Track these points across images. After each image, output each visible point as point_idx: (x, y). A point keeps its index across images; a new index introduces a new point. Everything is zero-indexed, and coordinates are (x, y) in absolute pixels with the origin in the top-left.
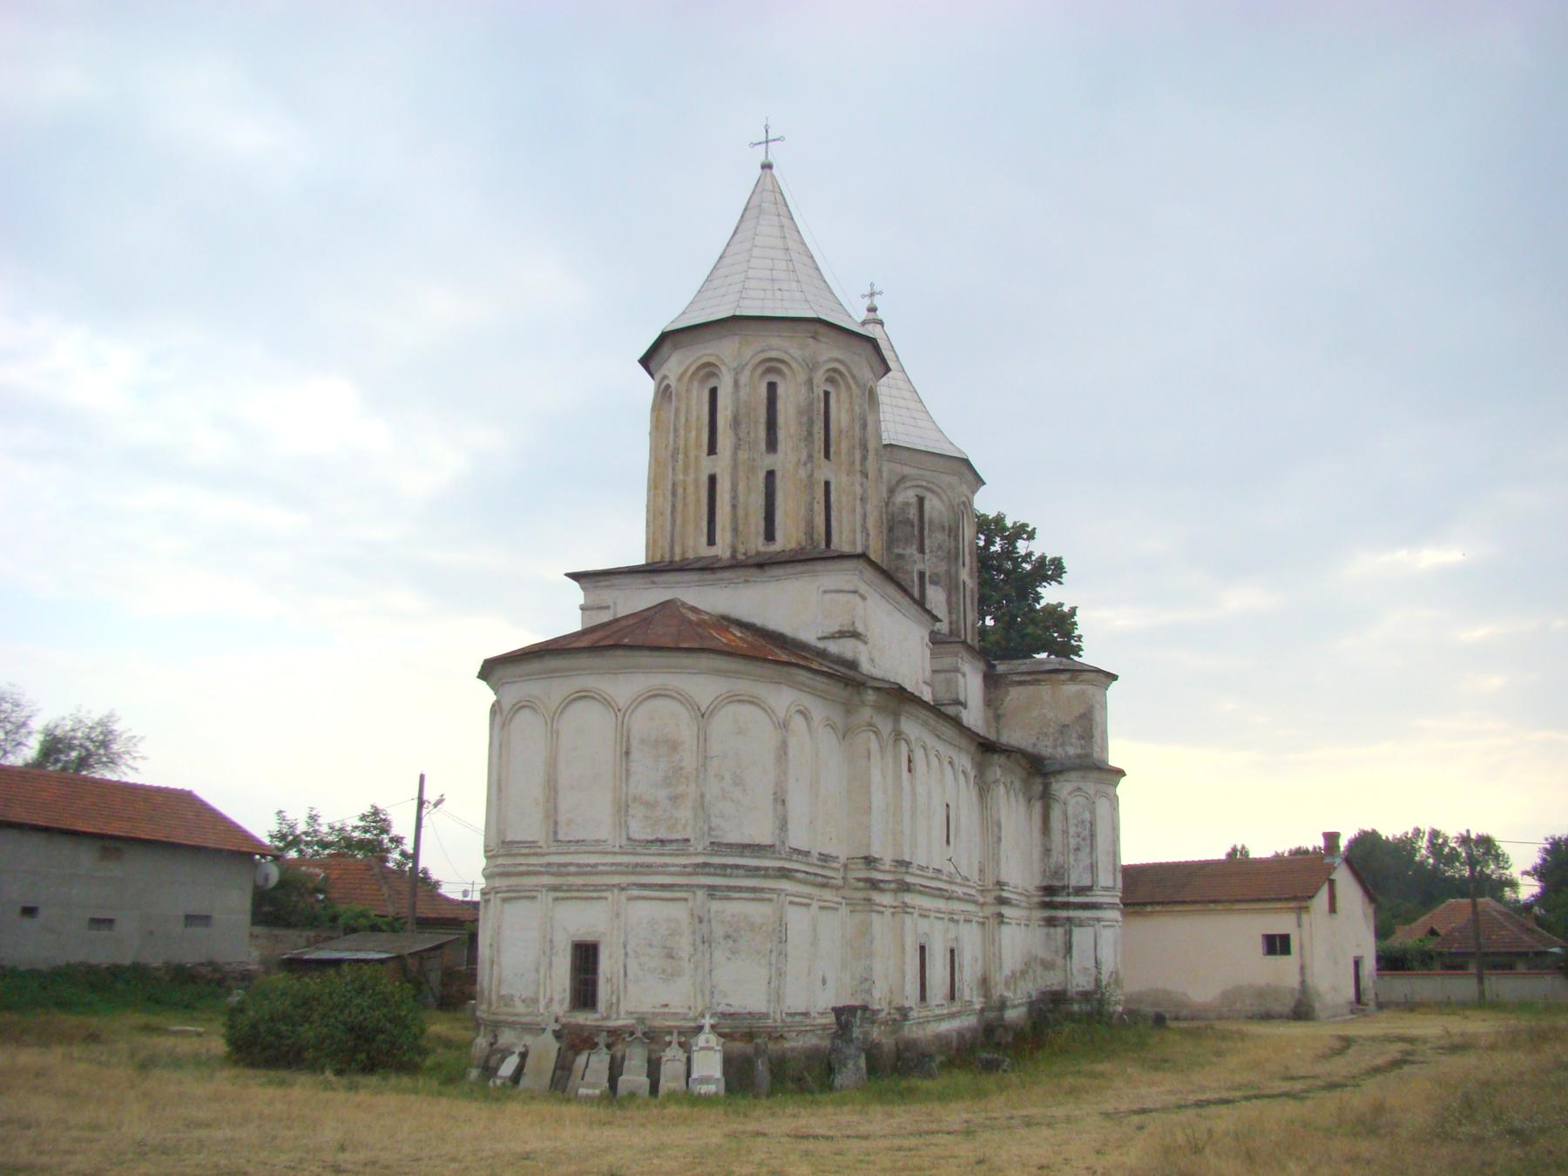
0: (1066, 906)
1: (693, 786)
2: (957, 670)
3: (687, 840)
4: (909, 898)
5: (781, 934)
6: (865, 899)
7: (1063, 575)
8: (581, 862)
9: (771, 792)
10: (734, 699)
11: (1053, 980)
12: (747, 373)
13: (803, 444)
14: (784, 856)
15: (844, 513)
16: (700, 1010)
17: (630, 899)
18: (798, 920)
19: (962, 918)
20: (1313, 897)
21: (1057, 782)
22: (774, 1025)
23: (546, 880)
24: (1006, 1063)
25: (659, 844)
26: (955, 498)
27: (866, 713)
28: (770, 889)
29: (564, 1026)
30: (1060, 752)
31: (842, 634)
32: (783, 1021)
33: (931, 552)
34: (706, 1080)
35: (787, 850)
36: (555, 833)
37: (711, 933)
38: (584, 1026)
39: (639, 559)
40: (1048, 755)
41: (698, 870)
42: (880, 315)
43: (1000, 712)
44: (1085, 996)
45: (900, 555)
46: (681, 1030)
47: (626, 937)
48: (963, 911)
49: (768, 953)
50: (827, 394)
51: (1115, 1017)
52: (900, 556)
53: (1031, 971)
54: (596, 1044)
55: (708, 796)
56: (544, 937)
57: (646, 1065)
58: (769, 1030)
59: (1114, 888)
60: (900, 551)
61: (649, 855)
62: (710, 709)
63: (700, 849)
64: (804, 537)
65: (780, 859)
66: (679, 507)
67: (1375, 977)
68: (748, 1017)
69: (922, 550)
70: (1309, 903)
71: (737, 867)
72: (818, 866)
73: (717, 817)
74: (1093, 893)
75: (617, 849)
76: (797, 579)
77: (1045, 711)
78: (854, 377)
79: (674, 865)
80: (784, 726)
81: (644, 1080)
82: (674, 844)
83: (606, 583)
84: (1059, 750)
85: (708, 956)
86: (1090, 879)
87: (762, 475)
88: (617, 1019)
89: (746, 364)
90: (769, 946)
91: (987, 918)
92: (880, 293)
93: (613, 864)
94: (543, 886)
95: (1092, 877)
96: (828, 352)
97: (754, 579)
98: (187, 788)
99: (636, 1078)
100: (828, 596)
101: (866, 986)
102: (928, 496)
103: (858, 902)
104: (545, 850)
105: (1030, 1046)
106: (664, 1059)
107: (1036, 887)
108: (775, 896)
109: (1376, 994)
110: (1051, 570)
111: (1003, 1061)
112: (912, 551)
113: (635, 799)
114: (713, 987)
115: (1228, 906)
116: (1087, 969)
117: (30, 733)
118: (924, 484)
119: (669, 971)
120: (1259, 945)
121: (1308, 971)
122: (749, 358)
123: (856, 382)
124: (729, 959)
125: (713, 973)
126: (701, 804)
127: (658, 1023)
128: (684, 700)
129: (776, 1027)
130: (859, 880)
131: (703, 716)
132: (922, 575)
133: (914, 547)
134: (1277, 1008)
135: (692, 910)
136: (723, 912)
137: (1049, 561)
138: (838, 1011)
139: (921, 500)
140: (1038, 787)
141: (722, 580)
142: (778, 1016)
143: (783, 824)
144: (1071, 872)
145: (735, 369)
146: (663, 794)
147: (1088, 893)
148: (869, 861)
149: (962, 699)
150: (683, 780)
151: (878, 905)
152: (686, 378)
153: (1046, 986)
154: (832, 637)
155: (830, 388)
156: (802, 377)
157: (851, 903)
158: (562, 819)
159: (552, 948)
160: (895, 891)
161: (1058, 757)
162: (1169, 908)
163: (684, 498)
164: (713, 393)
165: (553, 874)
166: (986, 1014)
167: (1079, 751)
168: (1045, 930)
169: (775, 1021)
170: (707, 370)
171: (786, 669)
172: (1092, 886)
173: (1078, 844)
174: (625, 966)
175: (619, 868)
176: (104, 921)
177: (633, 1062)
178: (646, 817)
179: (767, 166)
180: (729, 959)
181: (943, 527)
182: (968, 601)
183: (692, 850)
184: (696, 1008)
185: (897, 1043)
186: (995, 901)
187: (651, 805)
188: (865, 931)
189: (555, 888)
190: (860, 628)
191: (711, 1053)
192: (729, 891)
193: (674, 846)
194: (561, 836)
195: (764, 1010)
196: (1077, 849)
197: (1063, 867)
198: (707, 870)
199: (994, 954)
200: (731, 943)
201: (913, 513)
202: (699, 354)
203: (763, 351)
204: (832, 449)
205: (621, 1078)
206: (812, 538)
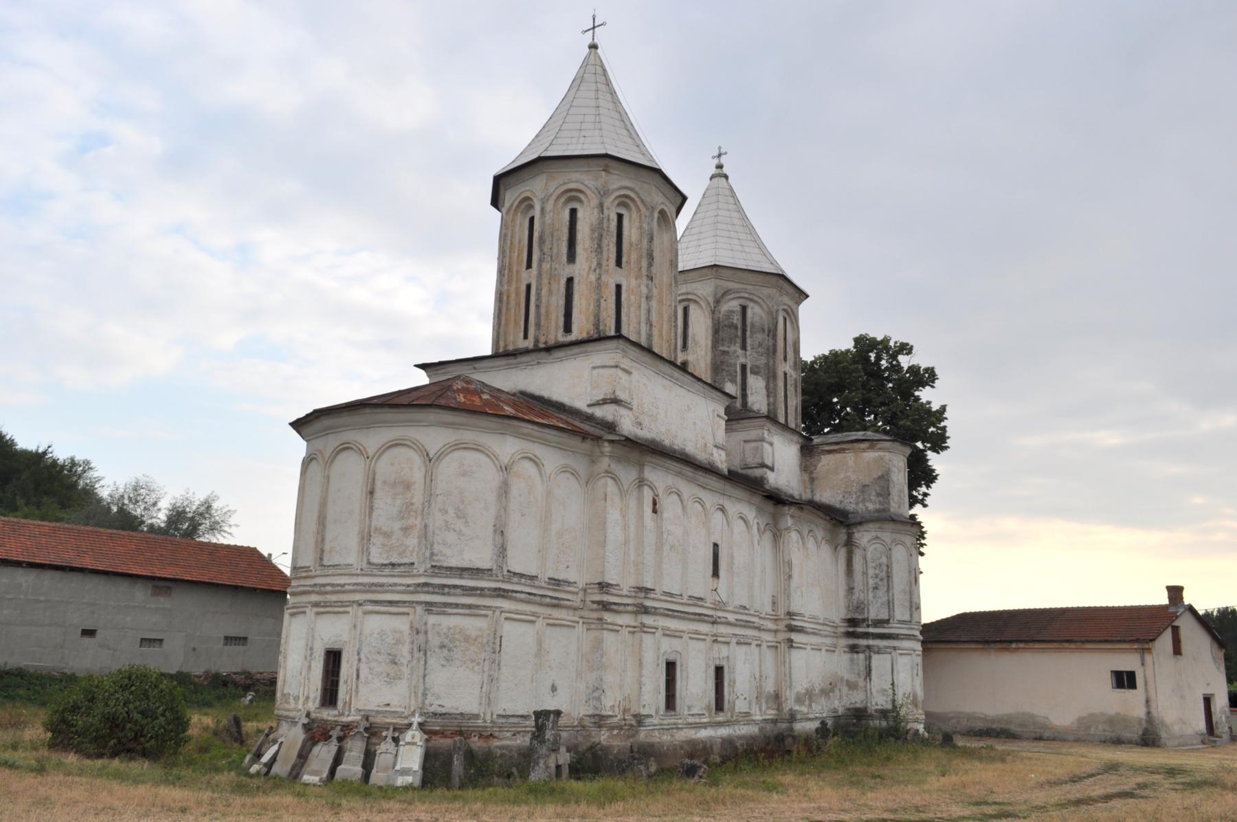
0: (866, 635)
1: (419, 518)
2: (763, 440)
3: (413, 564)
4: (648, 620)
5: (495, 645)
6: (598, 619)
7: (936, 381)
10: (458, 446)
11: (856, 699)
12: (551, 202)
13: (594, 255)
15: (632, 309)
16: (412, 709)
17: (365, 613)
18: (510, 631)
21: (859, 531)
22: (483, 724)
24: (703, 770)
25: (390, 567)
26: (773, 306)
27: (605, 462)
28: (484, 606)
29: (313, 721)
31: (605, 402)
32: (492, 722)
35: (505, 573)
36: (321, 559)
37: (426, 642)
38: (327, 721)
40: (852, 510)
41: (418, 589)
42: (725, 170)
43: (814, 475)
44: (884, 713)
46: (397, 726)
48: (734, 634)
50: (620, 217)
51: (911, 732)
52: (724, 353)
53: (837, 692)
54: (331, 736)
55: (430, 529)
56: (307, 645)
57: (362, 756)
58: (480, 729)
59: (910, 622)
63: (422, 571)
64: (592, 327)
65: (498, 581)
67: (1228, 713)
68: (459, 716)
69: (744, 347)
70: (1150, 645)
71: (455, 587)
72: (549, 589)
73: (439, 544)
74: (890, 625)
75: (359, 572)
77: (849, 474)
78: (642, 201)
79: (400, 585)
80: (506, 469)
81: (358, 770)
82: (402, 567)
83: (442, 371)
84: (861, 505)
85: (422, 662)
86: (887, 614)
87: (563, 281)
88: (348, 715)
91: (780, 643)
92: (726, 153)
95: (889, 612)
96: (618, 181)
97: (544, 361)
99: (352, 768)
100: (595, 372)
101: (596, 694)
102: (751, 305)
105: (763, 754)
106: (379, 752)
107: (842, 619)
108: (490, 613)
109: (1230, 728)
110: (926, 377)
111: (700, 767)
112: (736, 348)
113: (376, 529)
114: (425, 689)
115: (1079, 645)
116: (885, 690)
117: (159, 510)
118: (746, 295)
119: (392, 675)
120: (1108, 680)
121: (1153, 704)
124: (443, 666)
125: (426, 678)
126: (425, 534)
127: (379, 720)
129: (486, 727)
130: (593, 602)
131: (430, 461)
132: (744, 367)
133: (738, 345)
134: (1127, 735)
135: (411, 623)
137: (923, 370)
139: (744, 309)
140: (843, 537)
141: (523, 363)
142: (488, 718)
144: (871, 607)
145: (542, 199)
146: (397, 526)
147: (886, 625)
148: (603, 586)
149: (769, 463)
150: (412, 513)
151: (607, 624)
152: (512, 212)
153: (851, 704)
154: (597, 404)
155: (622, 211)
156: (595, 202)
157: (587, 622)
158: (327, 547)
160: (636, 613)
162: (1031, 645)
164: (532, 220)
165: (317, 593)
166: (779, 725)
168: (848, 656)
169: (485, 721)
170: (526, 203)
171: (507, 421)
172: (889, 620)
173: (876, 583)
174: (358, 671)
175: (359, 588)
176: (155, 640)
177: (353, 753)
178: (383, 545)
179: (593, 47)
180: (443, 666)
181: (763, 330)
182: (791, 389)
183: (415, 572)
184: (410, 708)
186: (785, 629)
187: (387, 535)
188: (598, 645)
189: (316, 605)
190: (622, 395)
191: (414, 747)
192: (445, 607)
193: (402, 569)
194: (326, 562)
195: (476, 712)
196: (876, 588)
197: (863, 603)
198: (426, 589)
199: (785, 675)
201: (736, 319)
203: (564, 184)
204: (624, 260)
205: (339, 768)
206: (598, 329)
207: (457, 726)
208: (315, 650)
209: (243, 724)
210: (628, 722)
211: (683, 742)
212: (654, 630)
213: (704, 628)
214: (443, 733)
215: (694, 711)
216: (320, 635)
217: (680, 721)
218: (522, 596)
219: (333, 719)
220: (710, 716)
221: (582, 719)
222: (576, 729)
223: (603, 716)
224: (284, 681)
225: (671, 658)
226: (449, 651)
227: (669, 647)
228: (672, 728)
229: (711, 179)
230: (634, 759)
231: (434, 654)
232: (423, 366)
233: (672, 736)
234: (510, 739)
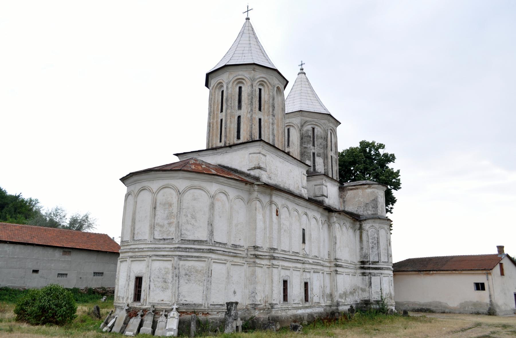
0: (369, 268)
2: (323, 185)
3: (173, 239)
4: (275, 262)
5: (209, 274)
7: (395, 160)
8: (139, 247)
9: (207, 221)
11: (365, 296)
12: (231, 84)
13: (249, 106)
14: (211, 244)
15: (266, 129)
16: (173, 302)
19: (312, 271)
20: (492, 269)
21: (364, 223)
23: (130, 254)
24: (300, 327)
25: (163, 240)
27: (255, 194)
28: (204, 257)
30: (365, 213)
31: (255, 168)
32: (208, 307)
33: (317, 146)
34: (170, 330)
35: (213, 242)
36: (133, 237)
39: (205, 148)
42: (304, 71)
44: (377, 302)
45: (305, 147)
46: (167, 310)
47: (151, 274)
49: (203, 281)
50: (260, 90)
52: (305, 148)
55: (180, 223)
56: (127, 275)
57: (152, 323)
60: (306, 146)
61: (160, 244)
62: (183, 192)
63: (177, 242)
66: (211, 131)
69: (314, 145)
70: (491, 271)
71: (191, 248)
73: (184, 230)
74: (379, 264)
75: (149, 242)
76: (242, 150)
77: (360, 199)
78: (270, 83)
81: (150, 329)
85: (177, 282)
86: (378, 259)
87: (236, 118)
88: (145, 305)
89: (231, 81)
90: (204, 278)
91: (332, 272)
92: (304, 64)
93: (148, 248)
94: (128, 256)
95: (379, 258)
96: (259, 75)
98: (105, 233)
99: (147, 328)
100: (251, 155)
103: (251, 263)
104: (130, 244)
106: (159, 321)
108: (207, 260)
110: (391, 158)
111: (299, 326)
112: (310, 146)
115: (460, 272)
116: (377, 292)
118: (314, 123)
119: (164, 287)
120: (473, 287)
121: (493, 297)
122: (231, 79)
123: (271, 85)
124: (186, 283)
125: (179, 288)
126: (178, 226)
128: (174, 189)
130: (251, 255)
131: (180, 194)
132: (314, 154)
134: (481, 310)
135: (173, 264)
136: (185, 265)
138: (228, 304)
139: (313, 129)
140: (358, 226)
141: (219, 152)
142: (206, 305)
143: (211, 233)
144: (370, 256)
146: (166, 222)
147: (377, 264)
148: (255, 248)
149: (325, 194)
154: (251, 169)
155: (261, 87)
156: (249, 84)
158: (136, 232)
159: (129, 279)
160: (270, 259)
161: (365, 215)
162: (439, 272)
163: (213, 127)
164: (223, 92)
166: (332, 307)
167: (373, 212)
168: (362, 277)
169: (205, 307)
170: (220, 85)
171: (213, 176)
172: (378, 261)
174: (149, 285)
176: (64, 274)
177: (147, 322)
178: (160, 231)
179: (248, 19)
180: (186, 283)
182: (334, 163)
183: (174, 242)
184: (172, 301)
185: (269, 317)
187: (162, 226)
188: (253, 274)
189: (131, 257)
190: (262, 165)
191: (174, 319)
192: (187, 257)
193: (168, 241)
194: (135, 239)
195: (201, 303)
196: (372, 248)
198: (179, 249)
199: (334, 286)
200: (187, 276)
201: (310, 133)
202: (217, 80)
204: (262, 108)
206: (251, 137)
207: (193, 310)
208: (131, 277)
209: (100, 310)
210: (267, 307)
211: (291, 315)
212: (278, 267)
213: (299, 265)
214: (186, 313)
215: (296, 302)
216: (133, 271)
217: (289, 306)
218: (221, 252)
219: (139, 307)
220: (303, 304)
221: (247, 306)
222: (245, 310)
223: (256, 304)
224: (118, 291)
225: (285, 279)
226: (189, 276)
227: (284, 274)
228: (286, 309)
229: (298, 75)
230: (270, 323)
231: (182, 278)
232: (177, 155)
233: (286, 313)
234: (216, 315)
